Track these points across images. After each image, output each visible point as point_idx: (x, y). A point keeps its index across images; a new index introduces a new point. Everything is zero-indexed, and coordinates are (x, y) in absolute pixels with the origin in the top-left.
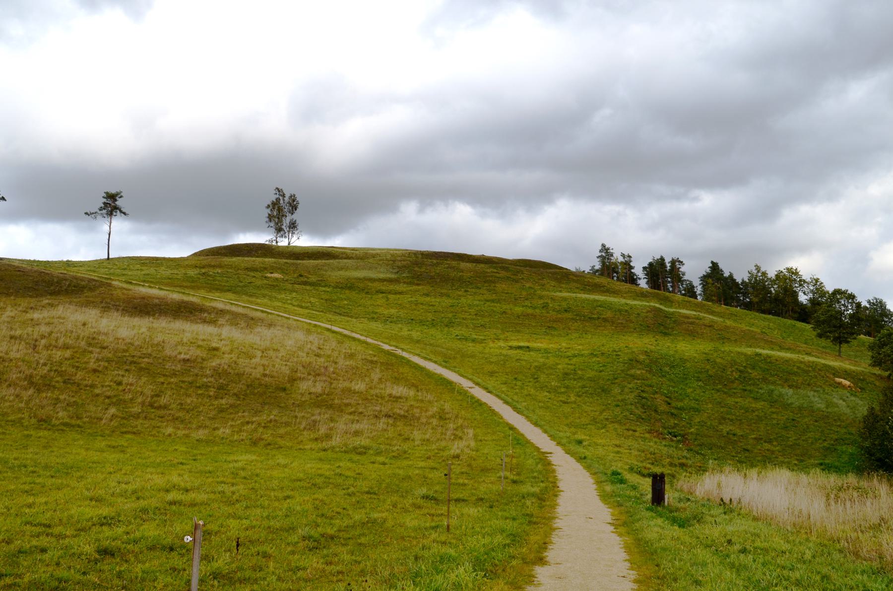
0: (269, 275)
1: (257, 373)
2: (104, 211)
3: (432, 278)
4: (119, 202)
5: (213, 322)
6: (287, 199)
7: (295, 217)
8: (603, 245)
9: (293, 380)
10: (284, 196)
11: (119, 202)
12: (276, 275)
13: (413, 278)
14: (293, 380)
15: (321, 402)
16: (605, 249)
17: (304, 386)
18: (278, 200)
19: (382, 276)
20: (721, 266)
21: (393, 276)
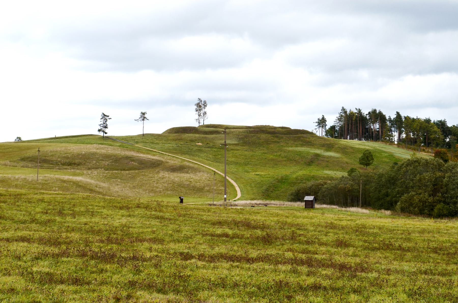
0: (197, 144)
1: (198, 186)
2: (141, 119)
3: (250, 143)
4: (146, 116)
5: (187, 172)
6: (202, 102)
7: (205, 110)
8: (343, 108)
9: (204, 187)
10: (201, 101)
11: (146, 116)
12: (200, 144)
13: (243, 143)
14: (204, 187)
15: (208, 191)
16: (343, 109)
17: (206, 188)
18: (199, 103)
19: (233, 142)
20: (400, 113)
21: (236, 142)
